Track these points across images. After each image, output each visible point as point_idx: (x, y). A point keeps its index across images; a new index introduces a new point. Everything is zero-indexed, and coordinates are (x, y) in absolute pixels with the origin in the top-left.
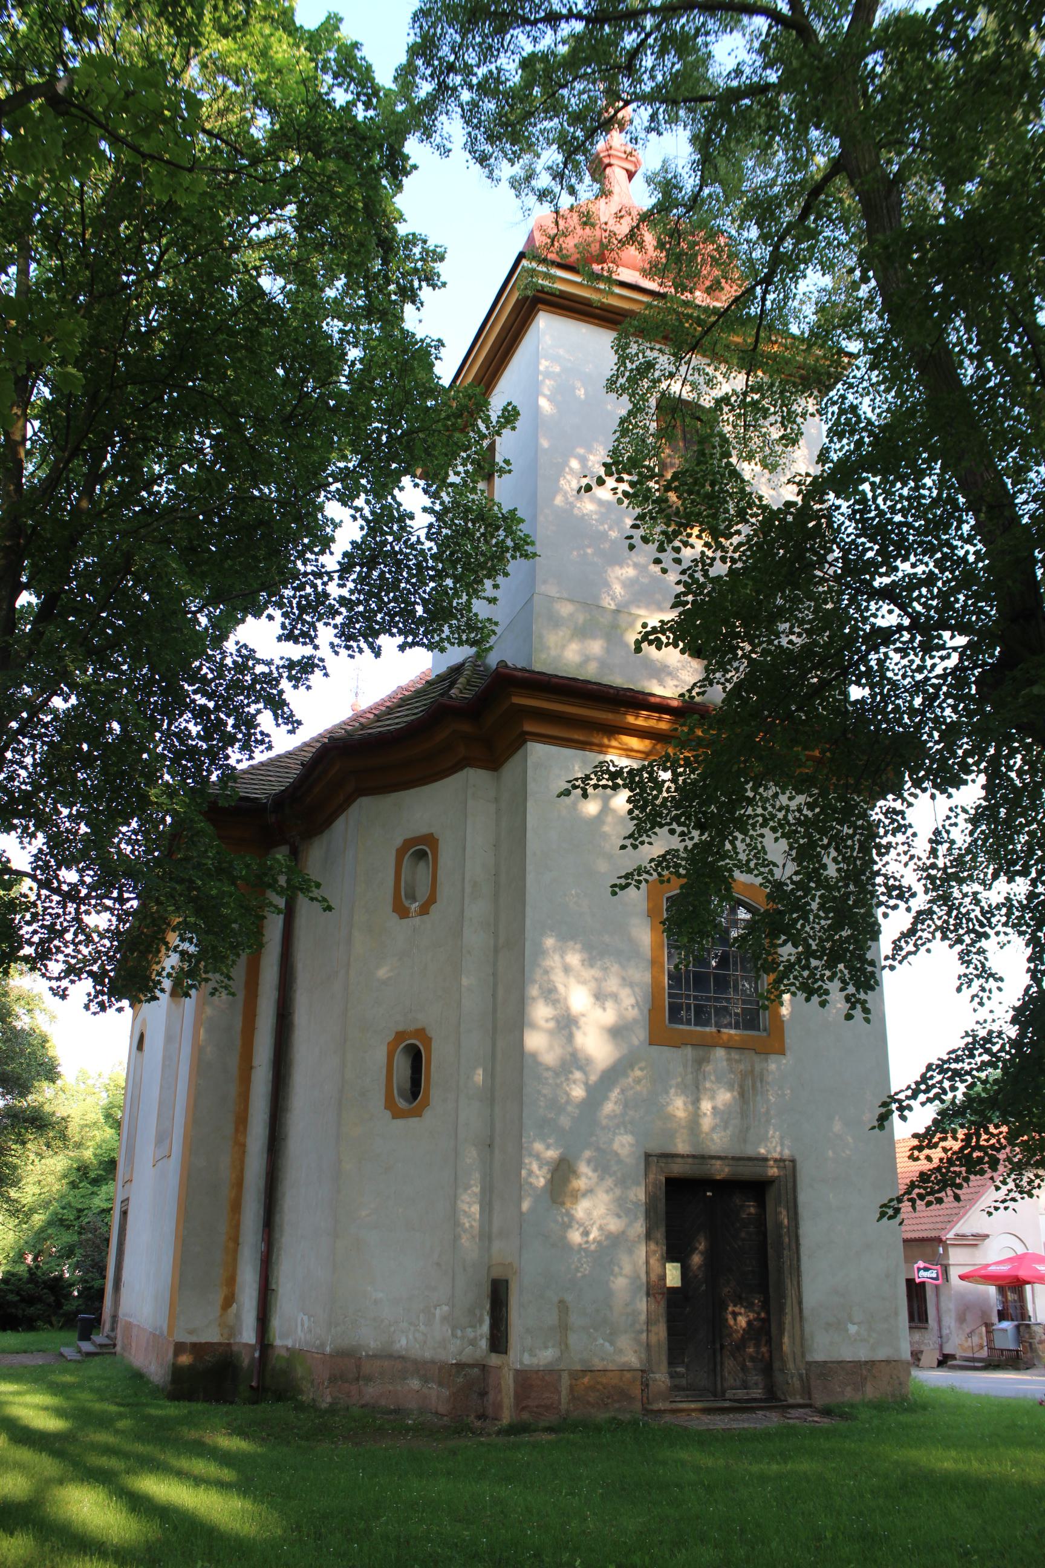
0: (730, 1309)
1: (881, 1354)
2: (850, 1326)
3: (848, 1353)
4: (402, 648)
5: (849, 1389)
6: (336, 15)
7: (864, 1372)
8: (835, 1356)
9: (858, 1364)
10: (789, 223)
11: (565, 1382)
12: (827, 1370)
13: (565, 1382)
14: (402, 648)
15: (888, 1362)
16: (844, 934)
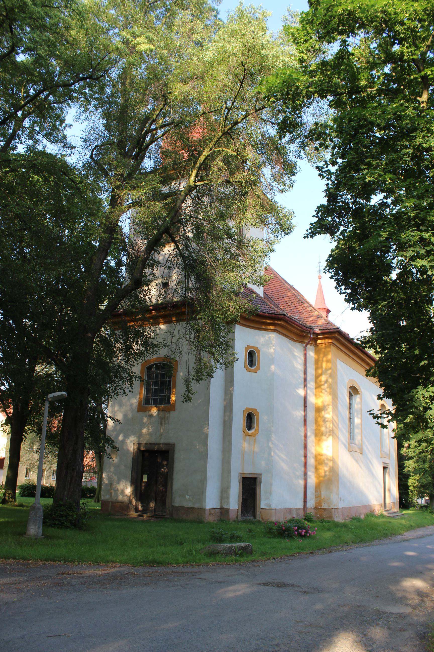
0: (417, 483)
1: (196, 506)
2: (187, 496)
3: (186, 504)
4: (352, 309)
5: (184, 515)
6: (289, 233)
7: (190, 511)
8: (181, 505)
9: (188, 508)
10: (223, 121)
11: (110, 504)
12: (178, 509)
13: (110, 504)
14: (352, 309)
15: (198, 508)
16: (362, 201)
